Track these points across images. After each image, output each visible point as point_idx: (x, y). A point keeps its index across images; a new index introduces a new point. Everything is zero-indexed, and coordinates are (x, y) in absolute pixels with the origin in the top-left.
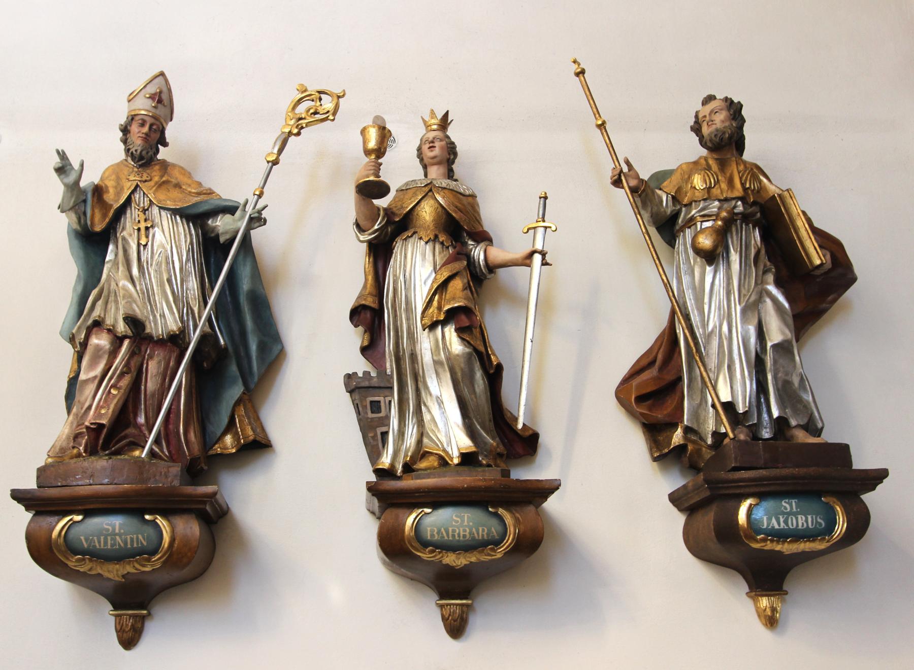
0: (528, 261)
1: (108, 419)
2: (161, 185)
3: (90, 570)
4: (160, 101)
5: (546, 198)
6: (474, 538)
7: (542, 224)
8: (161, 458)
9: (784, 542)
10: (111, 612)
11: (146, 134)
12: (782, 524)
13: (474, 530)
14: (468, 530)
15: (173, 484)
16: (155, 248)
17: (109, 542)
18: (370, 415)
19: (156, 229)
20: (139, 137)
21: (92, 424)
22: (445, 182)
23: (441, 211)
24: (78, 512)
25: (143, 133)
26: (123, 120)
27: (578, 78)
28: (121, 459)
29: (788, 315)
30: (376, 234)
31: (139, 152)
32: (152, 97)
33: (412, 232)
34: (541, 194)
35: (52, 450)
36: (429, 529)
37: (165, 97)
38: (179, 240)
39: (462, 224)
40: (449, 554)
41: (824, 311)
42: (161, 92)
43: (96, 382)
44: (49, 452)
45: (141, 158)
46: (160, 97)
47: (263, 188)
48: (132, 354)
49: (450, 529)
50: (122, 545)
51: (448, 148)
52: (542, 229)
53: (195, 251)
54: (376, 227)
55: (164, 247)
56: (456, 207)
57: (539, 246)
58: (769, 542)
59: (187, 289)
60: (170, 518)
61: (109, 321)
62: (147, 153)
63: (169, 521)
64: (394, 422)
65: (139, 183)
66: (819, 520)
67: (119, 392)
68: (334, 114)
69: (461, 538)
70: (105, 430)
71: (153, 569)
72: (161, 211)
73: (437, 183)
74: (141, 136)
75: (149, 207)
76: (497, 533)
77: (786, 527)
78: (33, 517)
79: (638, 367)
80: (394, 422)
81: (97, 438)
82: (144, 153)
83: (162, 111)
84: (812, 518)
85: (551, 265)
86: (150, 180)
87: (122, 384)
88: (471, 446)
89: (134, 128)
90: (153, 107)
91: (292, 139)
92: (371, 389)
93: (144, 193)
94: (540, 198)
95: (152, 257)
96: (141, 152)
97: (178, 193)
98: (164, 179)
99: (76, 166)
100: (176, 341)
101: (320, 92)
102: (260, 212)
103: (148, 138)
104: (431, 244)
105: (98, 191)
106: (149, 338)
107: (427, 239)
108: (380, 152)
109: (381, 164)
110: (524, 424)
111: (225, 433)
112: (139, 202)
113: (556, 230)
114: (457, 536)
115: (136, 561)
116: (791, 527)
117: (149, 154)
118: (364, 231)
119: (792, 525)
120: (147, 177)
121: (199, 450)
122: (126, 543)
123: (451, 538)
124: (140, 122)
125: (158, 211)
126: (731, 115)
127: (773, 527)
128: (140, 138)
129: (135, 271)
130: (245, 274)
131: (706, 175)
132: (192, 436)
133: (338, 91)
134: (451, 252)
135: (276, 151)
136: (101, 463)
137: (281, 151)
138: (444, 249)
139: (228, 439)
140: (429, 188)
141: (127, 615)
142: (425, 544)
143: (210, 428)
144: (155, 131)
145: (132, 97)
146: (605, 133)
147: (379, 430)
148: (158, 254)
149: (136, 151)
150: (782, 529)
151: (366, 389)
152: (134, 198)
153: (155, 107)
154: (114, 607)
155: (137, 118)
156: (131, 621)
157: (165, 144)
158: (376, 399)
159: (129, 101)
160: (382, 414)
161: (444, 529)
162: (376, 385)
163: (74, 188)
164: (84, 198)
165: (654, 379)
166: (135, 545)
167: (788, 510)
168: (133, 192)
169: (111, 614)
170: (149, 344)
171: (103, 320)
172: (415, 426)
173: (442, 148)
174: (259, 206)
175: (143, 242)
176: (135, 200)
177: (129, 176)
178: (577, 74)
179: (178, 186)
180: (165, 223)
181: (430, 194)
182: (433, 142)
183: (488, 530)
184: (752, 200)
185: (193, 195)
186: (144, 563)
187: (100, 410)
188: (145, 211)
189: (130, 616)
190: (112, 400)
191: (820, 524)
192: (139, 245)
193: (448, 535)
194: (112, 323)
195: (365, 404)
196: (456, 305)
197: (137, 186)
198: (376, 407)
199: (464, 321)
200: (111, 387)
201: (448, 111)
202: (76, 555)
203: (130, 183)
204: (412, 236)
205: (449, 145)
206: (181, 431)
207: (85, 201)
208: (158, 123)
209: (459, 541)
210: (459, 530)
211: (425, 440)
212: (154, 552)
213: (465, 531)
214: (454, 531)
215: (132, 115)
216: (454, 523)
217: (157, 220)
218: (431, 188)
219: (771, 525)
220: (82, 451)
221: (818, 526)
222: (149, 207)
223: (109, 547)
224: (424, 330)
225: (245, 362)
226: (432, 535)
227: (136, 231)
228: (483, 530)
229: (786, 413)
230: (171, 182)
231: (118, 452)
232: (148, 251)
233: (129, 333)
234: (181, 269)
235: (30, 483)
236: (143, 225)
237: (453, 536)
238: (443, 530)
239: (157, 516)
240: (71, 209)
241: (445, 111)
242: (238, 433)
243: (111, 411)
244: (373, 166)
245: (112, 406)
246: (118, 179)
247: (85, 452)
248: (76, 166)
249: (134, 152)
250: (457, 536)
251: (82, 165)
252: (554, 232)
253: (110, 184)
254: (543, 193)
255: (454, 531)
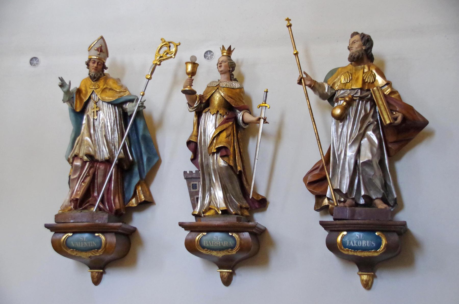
0: (258, 122)
1: (80, 196)
2: (103, 90)
3: (76, 254)
4: (101, 51)
5: (267, 92)
6: (222, 246)
7: (264, 105)
8: (104, 211)
9: (356, 252)
10: (89, 270)
11: (96, 67)
12: (355, 244)
13: (222, 242)
14: (220, 243)
15: (105, 222)
16: (100, 120)
17: (82, 244)
18: (192, 190)
19: (101, 111)
20: (93, 68)
21: (74, 198)
22: (225, 84)
23: (222, 98)
24: (71, 232)
25: (94, 67)
26: (87, 60)
27: (288, 28)
28: (85, 212)
29: (375, 147)
30: (195, 109)
31: (93, 75)
32: (97, 50)
33: (208, 110)
34: (265, 90)
35: (62, 206)
36: (205, 241)
37: (103, 49)
38: (111, 116)
39: (231, 104)
40: (213, 252)
41: (409, 140)
42: (101, 47)
43: (77, 179)
44: (61, 207)
45: (94, 78)
46: (101, 49)
47: (144, 91)
48: (90, 168)
49: (213, 242)
50: (87, 245)
51: (229, 65)
52: (265, 107)
53: (118, 120)
54: (195, 106)
55: (104, 120)
56: (229, 96)
57: (263, 116)
58: (350, 252)
59: (114, 138)
60: (104, 234)
61: (81, 155)
62: (97, 75)
63: (104, 236)
64: (200, 195)
65: (94, 90)
66: (372, 243)
67: (85, 184)
68: (175, 55)
69: (217, 246)
70: (79, 201)
71: (100, 255)
72: (103, 102)
73: (221, 85)
74: (94, 68)
75: (98, 101)
76: (232, 243)
77: (357, 245)
78: (54, 234)
79: (315, 168)
80: (200, 195)
81: (77, 203)
82: (96, 75)
83: (102, 55)
84: (369, 242)
85: (269, 123)
86: (99, 88)
87: (86, 181)
88: (224, 207)
89: (91, 64)
90: (98, 54)
91: (157, 66)
92: (193, 179)
93: (96, 95)
94: (265, 92)
95: (99, 125)
96: (94, 75)
97: (111, 93)
98: (105, 87)
99: (68, 83)
100: (108, 162)
101: (169, 43)
102: (142, 103)
103: (97, 69)
104: (215, 116)
105: (79, 91)
106: (97, 161)
107: (213, 113)
108: (193, 73)
109: (193, 80)
110: (252, 197)
111: (132, 198)
112: (94, 98)
113: (269, 108)
114: (215, 245)
115: (93, 251)
116: (359, 246)
117: (98, 75)
118: (191, 106)
119: (360, 245)
120: (98, 87)
121: (221, 165)
122: (88, 244)
123: (213, 245)
124: (93, 61)
125: (102, 103)
126: (363, 43)
127: (351, 245)
128: (93, 69)
129: (92, 131)
130: (141, 126)
131: (346, 76)
132: (117, 200)
133: (177, 43)
134: (225, 118)
135: (150, 74)
136: (77, 213)
137: (152, 73)
138: (222, 117)
139: (134, 200)
140: (217, 87)
141: (95, 272)
142: (204, 248)
143: (127, 196)
144: (100, 65)
145: (90, 48)
146: (297, 58)
147: (196, 197)
148: (101, 123)
149: (92, 75)
150: (355, 246)
151: (190, 179)
152: (92, 96)
153: (99, 54)
154: (90, 268)
155: (92, 60)
156: (97, 274)
157: (106, 68)
158: (195, 183)
159: (89, 51)
160: (196, 190)
161: (210, 242)
162: (194, 177)
163: (67, 93)
164: (72, 96)
165: (317, 174)
166: (92, 246)
167: (359, 238)
168: (91, 94)
169: (89, 271)
170: (98, 163)
171: (79, 154)
172: (209, 196)
173: (225, 66)
174: (142, 100)
175: (96, 118)
176: (93, 98)
177: (90, 86)
178: (288, 26)
179: (111, 89)
180: (105, 108)
181: (217, 90)
182: (220, 64)
183: (228, 242)
184: (366, 89)
185: (118, 93)
186: (96, 252)
187: (78, 192)
188: (96, 103)
189: (96, 272)
190: (82, 187)
191: (373, 245)
192: (94, 119)
193: (212, 244)
194: (82, 156)
195: (190, 185)
196: (220, 146)
197: (93, 91)
198: (195, 187)
199: (224, 153)
200: (82, 183)
201: (230, 46)
202: (70, 249)
203: (90, 90)
204: (208, 111)
205: (229, 64)
206: (112, 198)
207: (73, 97)
208: (101, 61)
209: (216, 247)
210: (216, 242)
211: (212, 202)
212: (99, 248)
213: (218, 243)
214: (214, 243)
215: (90, 58)
216: (214, 239)
217: (101, 107)
218: (218, 87)
219: (350, 244)
220: (73, 208)
221: (371, 245)
222: (98, 101)
223: (82, 246)
224: (210, 155)
225: (142, 166)
226: (206, 244)
227: (93, 113)
228: (226, 243)
229: (339, 198)
230: (108, 88)
231: (85, 209)
232: (97, 122)
233: (88, 160)
234: (111, 129)
235: (52, 221)
236: (95, 110)
237: (214, 244)
238: (210, 242)
239: (100, 234)
240: (67, 101)
241: (229, 46)
242: (138, 198)
243: (81, 192)
244: (189, 81)
245: (82, 191)
246: (86, 87)
247: (74, 208)
248: (68, 83)
249: (91, 76)
250: (215, 245)
251: (70, 83)
252: (270, 108)
253: (83, 89)
254: (266, 90)
255: (214, 243)
